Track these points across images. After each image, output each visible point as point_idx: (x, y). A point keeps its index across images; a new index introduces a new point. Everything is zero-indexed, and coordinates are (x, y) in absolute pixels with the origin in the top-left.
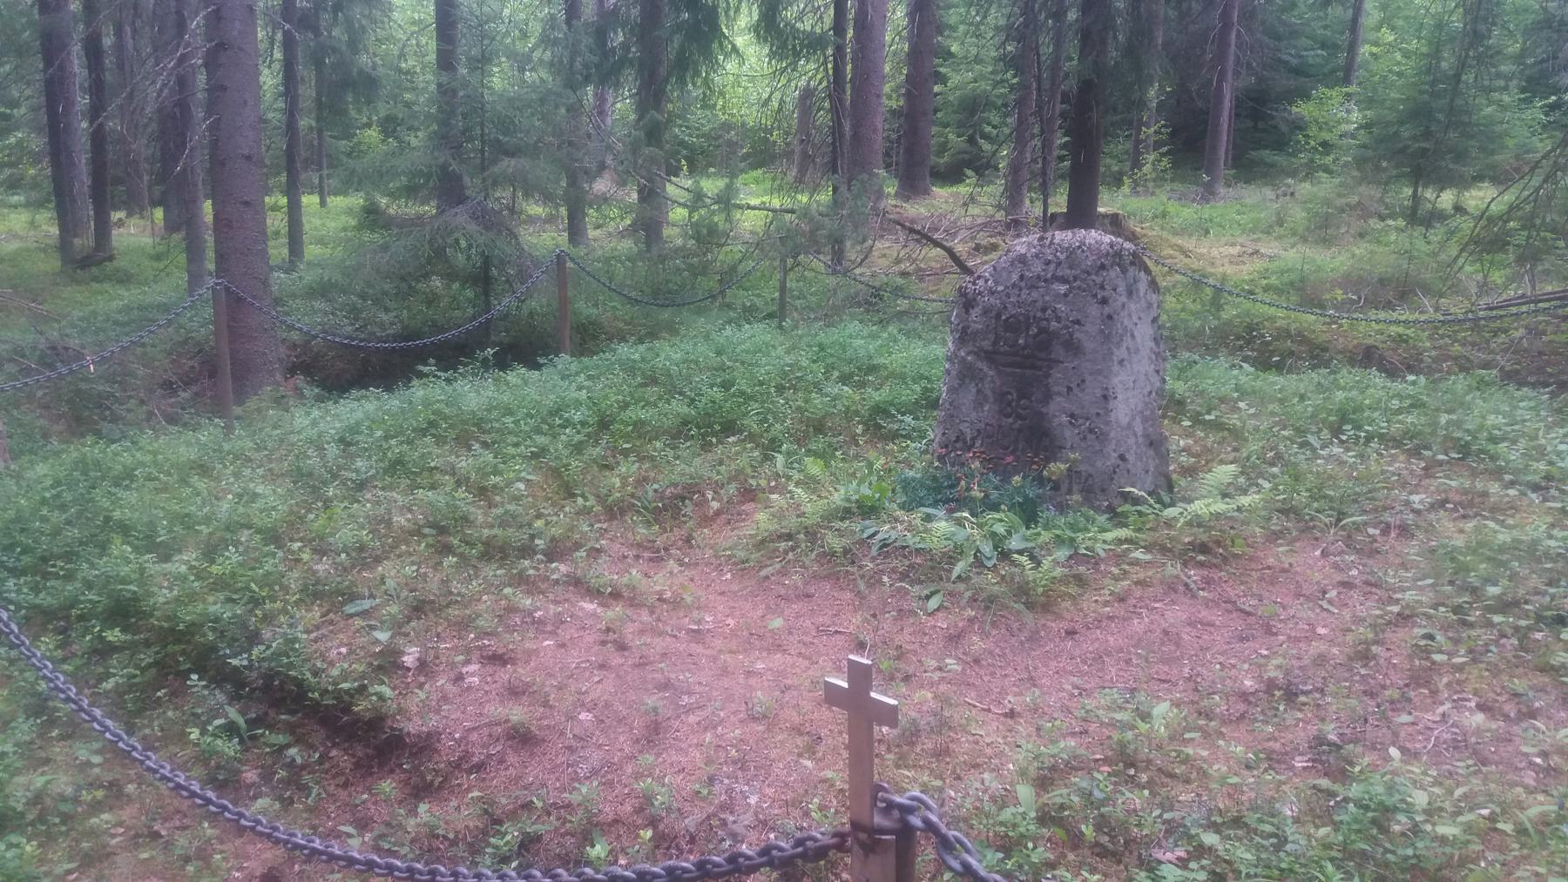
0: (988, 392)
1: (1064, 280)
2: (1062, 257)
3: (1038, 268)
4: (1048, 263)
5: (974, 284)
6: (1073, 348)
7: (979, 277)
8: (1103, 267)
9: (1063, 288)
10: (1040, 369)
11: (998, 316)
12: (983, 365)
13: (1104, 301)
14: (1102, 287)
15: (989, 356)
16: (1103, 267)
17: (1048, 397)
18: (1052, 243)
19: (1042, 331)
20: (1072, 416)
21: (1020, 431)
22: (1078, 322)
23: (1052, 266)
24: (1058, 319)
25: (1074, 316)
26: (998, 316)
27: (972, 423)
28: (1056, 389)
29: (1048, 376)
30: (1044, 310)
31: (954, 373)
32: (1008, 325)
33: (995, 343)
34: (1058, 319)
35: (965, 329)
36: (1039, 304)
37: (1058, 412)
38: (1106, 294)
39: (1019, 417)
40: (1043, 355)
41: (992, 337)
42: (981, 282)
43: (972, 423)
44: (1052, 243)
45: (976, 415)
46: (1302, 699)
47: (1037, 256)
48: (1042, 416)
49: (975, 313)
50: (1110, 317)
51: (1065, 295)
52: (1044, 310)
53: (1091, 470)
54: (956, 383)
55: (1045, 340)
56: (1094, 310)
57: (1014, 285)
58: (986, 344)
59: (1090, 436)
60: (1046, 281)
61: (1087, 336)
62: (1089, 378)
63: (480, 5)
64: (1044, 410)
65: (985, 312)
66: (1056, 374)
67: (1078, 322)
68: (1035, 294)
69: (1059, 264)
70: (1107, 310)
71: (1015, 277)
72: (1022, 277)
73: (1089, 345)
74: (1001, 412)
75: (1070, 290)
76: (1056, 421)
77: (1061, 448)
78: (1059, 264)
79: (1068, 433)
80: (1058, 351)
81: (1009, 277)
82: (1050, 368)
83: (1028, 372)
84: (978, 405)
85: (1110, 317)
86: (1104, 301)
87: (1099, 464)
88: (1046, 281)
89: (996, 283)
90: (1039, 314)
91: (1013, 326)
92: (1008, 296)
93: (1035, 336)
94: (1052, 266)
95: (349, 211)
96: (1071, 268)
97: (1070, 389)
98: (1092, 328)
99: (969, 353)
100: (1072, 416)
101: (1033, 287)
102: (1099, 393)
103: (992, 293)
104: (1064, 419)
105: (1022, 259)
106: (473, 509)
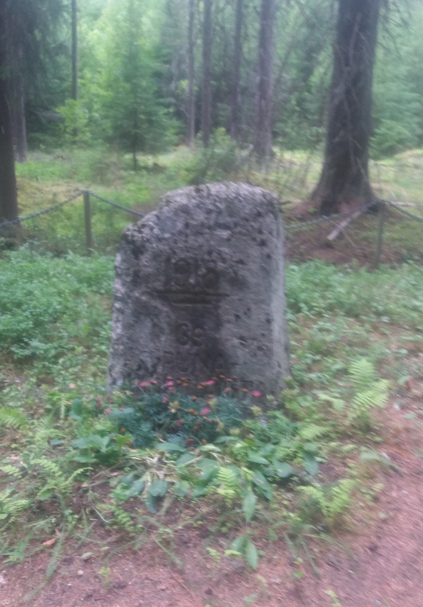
0: (164, 326)
1: (226, 227)
2: (222, 206)
3: (201, 216)
4: (209, 212)
5: (140, 232)
6: (238, 283)
7: (144, 226)
9: (225, 234)
10: (209, 302)
11: (168, 260)
12: (157, 303)
13: (263, 243)
14: (260, 232)
15: (163, 295)
16: (259, 214)
17: (219, 325)
18: (209, 195)
19: (211, 270)
20: (242, 338)
21: (196, 354)
22: (241, 262)
24: (224, 260)
25: (238, 256)
26: (168, 260)
27: (151, 352)
29: (217, 307)
30: (210, 253)
31: (128, 311)
33: (167, 283)
34: (224, 260)
35: (136, 274)
36: (205, 248)
37: (229, 336)
38: (264, 237)
39: (195, 343)
40: (211, 291)
41: (162, 278)
42: (146, 231)
43: (151, 352)
45: (152, 346)
46: (242, 406)
47: (198, 206)
49: (145, 259)
50: (269, 257)
51: (228, 240)
52: (210, 253)
53: (262, 379)
54: (131, 320)
55: (213, 278)
56: (255, 252)
57: (180, 233)
58: (158, 285)
59: (260, 353)
60: (210, 228)
61: (250, 273)
64: (217, 336)
65: (156, 256)
66: (224, 305)
67: (241, 262)
68: (201, 240)
70: (266, 250)
71: (180, 225)
72: (187, 225)
73: (252, 280)
77: (234, 364)
79: (240, 352)
80: (225, 287)
82: (218, 301)
83: (199, 306)
84: (155, 336)
86: (263, 243)
88: (210, 228)
89: (163, 230)
90: (206, 257)
91: (185, 267)
92: (176, 242)
93: (204, 276)
94: (213, 216)
95: (59, 109)
98: (254, 266)
99: (143, 293)
100: (242, 338)
101: (199, 233)
102: (263, 318)
103: (159, 239)
104: (236, 341)
105: (184, 210)
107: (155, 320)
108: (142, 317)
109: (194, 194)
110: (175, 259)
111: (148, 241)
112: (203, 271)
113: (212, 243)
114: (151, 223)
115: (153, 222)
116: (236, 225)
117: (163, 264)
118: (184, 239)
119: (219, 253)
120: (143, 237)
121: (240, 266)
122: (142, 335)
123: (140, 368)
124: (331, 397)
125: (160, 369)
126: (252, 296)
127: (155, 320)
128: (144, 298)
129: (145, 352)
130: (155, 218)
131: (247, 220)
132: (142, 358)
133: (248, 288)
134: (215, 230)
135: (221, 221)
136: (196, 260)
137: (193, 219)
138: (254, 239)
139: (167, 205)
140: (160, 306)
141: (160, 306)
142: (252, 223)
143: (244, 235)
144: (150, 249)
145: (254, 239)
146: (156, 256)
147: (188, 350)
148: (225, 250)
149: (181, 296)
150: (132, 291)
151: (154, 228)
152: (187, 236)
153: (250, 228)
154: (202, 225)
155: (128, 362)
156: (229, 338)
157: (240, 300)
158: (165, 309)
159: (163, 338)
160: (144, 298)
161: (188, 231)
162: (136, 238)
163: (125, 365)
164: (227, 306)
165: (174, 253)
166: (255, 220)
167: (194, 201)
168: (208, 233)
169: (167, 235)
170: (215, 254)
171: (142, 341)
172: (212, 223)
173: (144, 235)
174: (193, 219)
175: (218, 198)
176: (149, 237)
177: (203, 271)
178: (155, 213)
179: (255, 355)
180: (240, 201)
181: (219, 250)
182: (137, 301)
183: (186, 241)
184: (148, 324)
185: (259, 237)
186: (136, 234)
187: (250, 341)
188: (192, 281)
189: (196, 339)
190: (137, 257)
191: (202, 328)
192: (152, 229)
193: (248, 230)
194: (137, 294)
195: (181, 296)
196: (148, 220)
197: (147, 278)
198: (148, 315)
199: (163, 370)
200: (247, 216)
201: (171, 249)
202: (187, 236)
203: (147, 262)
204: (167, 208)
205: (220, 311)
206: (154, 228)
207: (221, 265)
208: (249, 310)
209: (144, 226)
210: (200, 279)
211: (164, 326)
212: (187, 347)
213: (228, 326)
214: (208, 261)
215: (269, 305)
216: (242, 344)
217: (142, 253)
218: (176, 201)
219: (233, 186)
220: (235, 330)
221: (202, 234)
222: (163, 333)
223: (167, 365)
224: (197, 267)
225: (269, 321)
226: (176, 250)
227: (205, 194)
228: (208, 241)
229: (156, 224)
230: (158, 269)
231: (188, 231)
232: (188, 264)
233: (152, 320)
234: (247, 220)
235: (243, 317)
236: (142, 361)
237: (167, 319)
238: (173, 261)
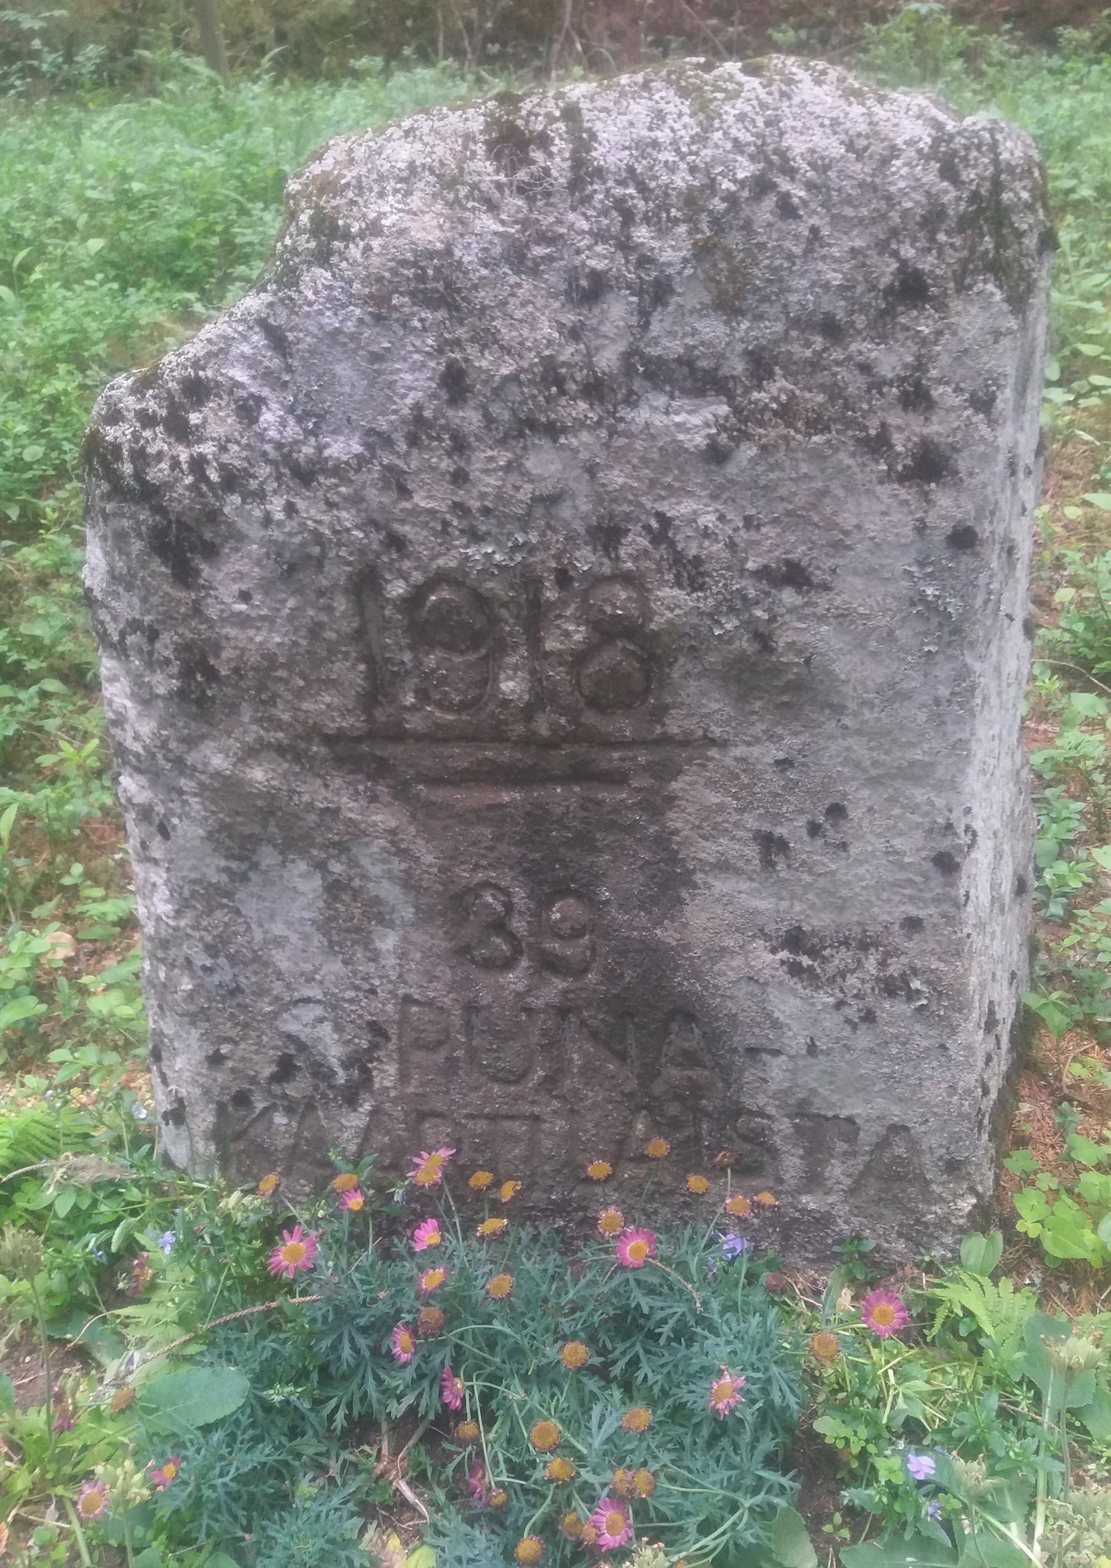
1: (697, 379)
2: (671, 251)
3: (535, 322)
4: (590, 290)
5: (180, 430)
6: (773, 681)
8: (912, 289)
9: (695, 421)
10: (618, 779)
11: (366, 582)
14: (916, 397)
15: (365, 751)
16: (912, 289)
17: (670, 881)
18: (583, 173)
20: (795, 940)
22: (794, 575)
23: (617, 310)
24: (691, 573)
26: (366, 582)
28: (708, 850)
29: (658, 804)
30: (607, 535)
32: (423, 623)
33: (377, 690)
34: (691, 573)
36: (578, 510)
37: (727, 925)
38: (936, 428)
39: (550, 965)
40: (625, 726)
41: (350, 672)
42: (214, 420)
43: (332, 1004)
44: (583, 173)
47: (516, 256)
48: (657, 961)
49: (229, 581)
50: (963, 539)
51: (716, 455)
52: (607, 535)
55: (634, 665)
56: (880, 514)
57: (419, 428)
59: (890, 1008)
62: (861, 800)
63: (1056, 464)
64: (666, 934)
65: (292, 567)
66: (695, 792)
67: (794, 575)
68: (545, 464)
69: (657, 293)
70: (947, 506)
71: (414, 383)
72: (455, 383)
73: (852, 668)
74: (464, 951)
75: (743, 423)
76: (729, 970)
78: (657, 293)
80: (698, 702)
81: (378, 382)
82: (665, 772)
83: (561, 797)
84: (348, 917)
85: (963, 539)
86: (930, 467)
87: (935, 1093)
89: (312, 416)
90: (586, 559)
91: (467, 621)
93: (579, 658)
94: (617, 310)
96: (728, 305)
97: (771, 846)
99: (252, 753)
101: (530, 427)
102: (913, 847)
104: (766, 959)
105: (434, 286)
106: (168, 325)
107: (337, 867)
108: (268, 857)
109: (484, 170)
110: (404, 576)
111: (232, 480)
112: (569, 633)
113: (616, 478)
114: (240, 375)
115: (251, 363)
116: (761, 364)
117: (341, 604)
118: (446, 464)
119: (662, 531)
120: (198, 464)
121: (788, 596)
122: (278, 929)
123: (286, 1069)
124: (1011, 565)
125: (386, 1075)
126: (859, 747)
127: (337, 867)
128: (258, 774)
129: (307, 1000)
130: (258, 338)
131: (832, 330)
132: (292, 1028)
133: (838, 709)
134: (631, 400)
135: (667, 340)
136: (528, 581)
137: (487, 339)
138: (878, 444)
139: (323, 257)
140: (350, 807)
141: (350, 807)
142: (862, 347)
143: (817, 424)
144: (255, 532)
145: (878, 444)
146: (292, 567)
147: (519, 995)
148: (695, 510)
149: (460, 757)
150: (192, 742)
151: (260, 401)
152: (460, 445)
153: (854, 383)
154: (552, 376)
155: (225, 1049)
156: (729, 942)
157: (784, 764)
158: (383, 818)
159: (388, 942)
160: (258, 774)
161: (469, 418)
162: (159, 472)
163: (215, 1060)
164: (714, 798)
165: (396, 543)
166: (882, 326)
167: (487, 223)
168: (580, 424)
169: (341, 447)
170: (635, 541)
171: (281, 960)
172: (608, 359)
173: (207, 449)
174: (487, 339)
175: (639, 200)
176: (234, 456)
177: (569, 633)
178: (254, 303)
179: (869, 1017)
180: (787, 209)
181: (661, 516)
182: (225, 790)
183: (460, 478)
184: (304, 885)
185: (907, 432)
186: (157, 441)
187: (842, 958)
188: (510, 686)
189: (555, 946)
190: (185, 576)
191: (585, 895)
192: (248, 410)
193: (835, 392)
194: (218, 762)
195: (460, 757)
196: (220, 352)
197: (262, 680)
198: (294, 843)
199: (404, 1076)
200: (839, 308)
201: (371, 523)
202: (460, 445)
203: (245, 597)
204: (323, 275)
205: (675, 820)
206: (260, 401)
207: (671, 602)
208: (837, 811)
209: (197, 390)
210: (557, 673)
211: (390, 892)
212: (515, 979)
213: (720, 885)
214: (596, 580)
215: (952, 786)
216: (795, 970)
217: (211, 552)
218: (374, 228)
219: (742, 92)
220: (763, 904)
221: (553, 431)
222: (383, 921)
223: (418, 1056)
224: (536, 616)
225: (947, 864)
226: (406, 529)
227: (557, 164)
228: (591, 470)
229: (268, 377)
230: (315, 631)
231: (469, 418)
232: (482, 601)
233: (321, 866)
234: (832, 330)
235: (803, 847)
236: (290, 1038)
237: (398, 866)
238: (397, 589)
